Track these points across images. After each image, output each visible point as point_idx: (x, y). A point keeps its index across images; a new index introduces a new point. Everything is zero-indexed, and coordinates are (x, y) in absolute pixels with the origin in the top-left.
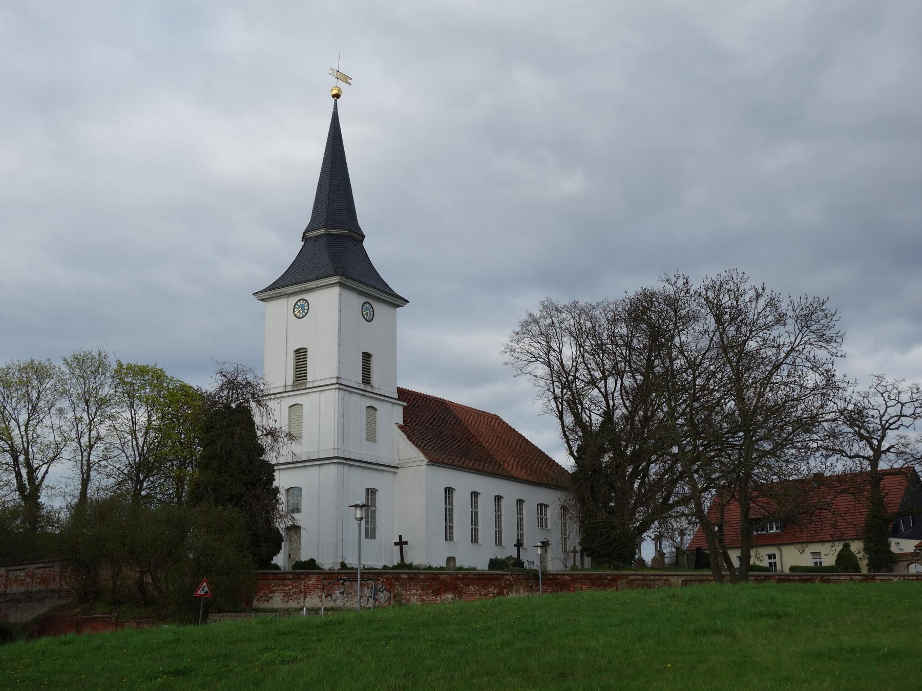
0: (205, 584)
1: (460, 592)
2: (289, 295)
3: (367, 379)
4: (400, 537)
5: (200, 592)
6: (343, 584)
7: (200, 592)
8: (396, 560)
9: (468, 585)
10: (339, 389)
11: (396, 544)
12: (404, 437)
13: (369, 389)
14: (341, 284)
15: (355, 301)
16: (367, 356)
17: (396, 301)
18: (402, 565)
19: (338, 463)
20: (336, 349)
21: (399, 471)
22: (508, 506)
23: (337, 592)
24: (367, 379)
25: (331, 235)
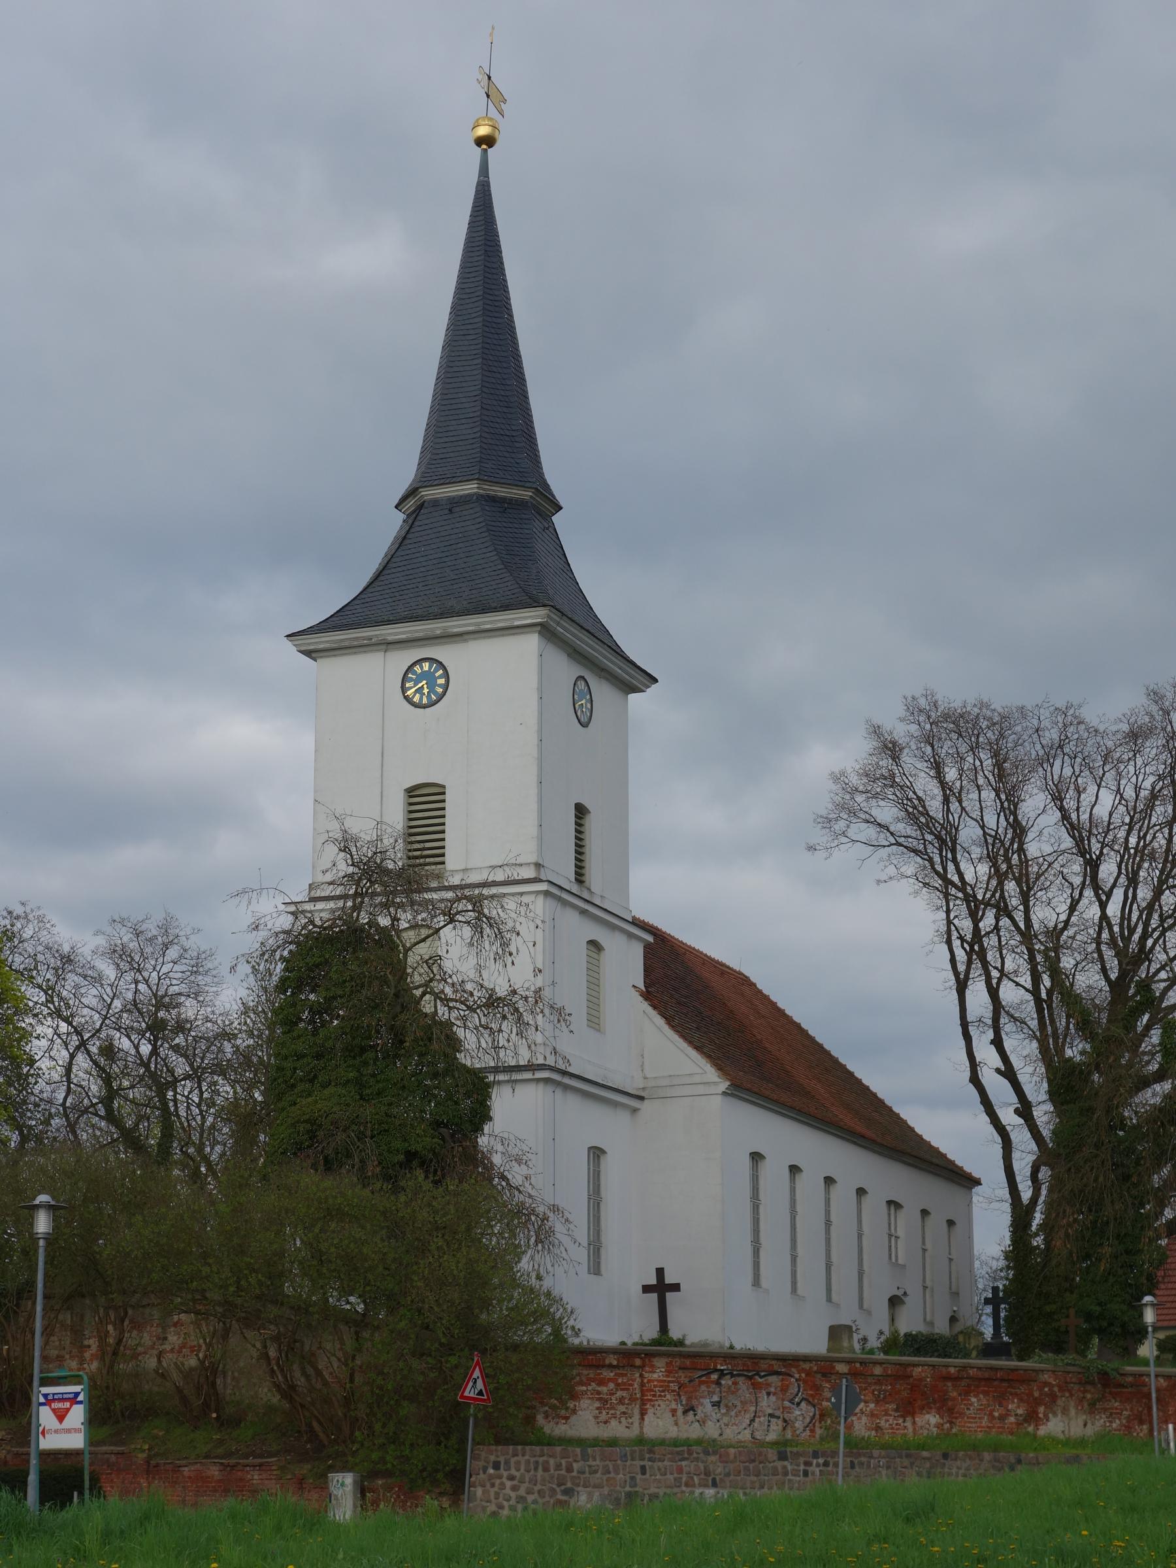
0: (477, 1373)
1: (951, 1411)
2: (388, 645)
3: (580, 878)
4: (660, 1272)
5: (469, 1392)
6: (718, 1383)
7: (469, 1392)
8: (651, 1332)
9: (967, 1393)
10: (547, 893)
11: (647, 1289)
12: (660, 1021)
13: (586, 895)
14: (545, 630)
15: (565, 671)
16: (581, 811)
17: (632, 678)
18: (664, 1344)
19: (547, 1081)
20: (533, 791)
21: (645, 1106)
22: (774, 1174)
23: (707, 1402)
24: (580, 878)
25: (492, 500)
